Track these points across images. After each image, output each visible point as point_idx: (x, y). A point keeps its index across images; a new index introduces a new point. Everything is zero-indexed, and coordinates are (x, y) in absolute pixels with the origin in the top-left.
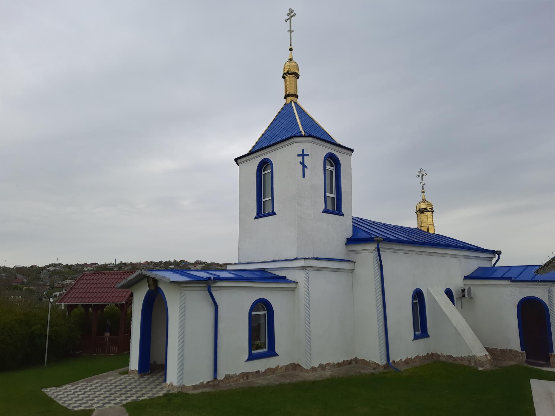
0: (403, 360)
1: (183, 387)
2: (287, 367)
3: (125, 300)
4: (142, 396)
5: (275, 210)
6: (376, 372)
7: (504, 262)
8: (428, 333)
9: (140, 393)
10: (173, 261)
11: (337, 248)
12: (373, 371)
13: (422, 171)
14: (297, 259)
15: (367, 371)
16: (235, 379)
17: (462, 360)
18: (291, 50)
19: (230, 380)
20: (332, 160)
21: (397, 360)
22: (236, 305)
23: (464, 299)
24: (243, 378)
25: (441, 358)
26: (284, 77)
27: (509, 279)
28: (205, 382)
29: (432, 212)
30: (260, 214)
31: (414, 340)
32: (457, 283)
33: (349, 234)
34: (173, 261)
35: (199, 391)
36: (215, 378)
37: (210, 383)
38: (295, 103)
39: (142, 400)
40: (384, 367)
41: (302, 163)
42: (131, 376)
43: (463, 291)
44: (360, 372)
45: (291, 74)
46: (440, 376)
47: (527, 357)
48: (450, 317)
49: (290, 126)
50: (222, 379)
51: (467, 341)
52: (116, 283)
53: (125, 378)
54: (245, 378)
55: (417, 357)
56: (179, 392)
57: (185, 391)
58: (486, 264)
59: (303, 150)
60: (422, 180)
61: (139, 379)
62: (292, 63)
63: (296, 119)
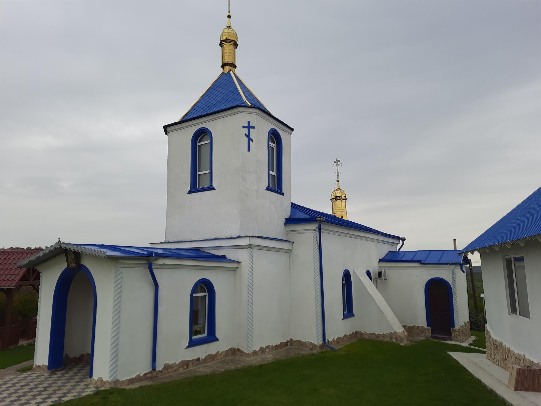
0: (335, 339)
1: (117, 381)
2: (227, 353)
3: (14, 283)
4: (65, 396)
5: (214, 185)
6: (315, 351)
7: (408, 247)
8: (354, 312)
9: (60, 393)
10: (44, 248)
11: (276, 227)
12: (310, 352)
13: (337, 161)
14: (239, 237)
15: (306, 352)
16: (175, 368)
17: (383, 337)
18: (229, 17)
19: (169, 370)
20: (275, 137)
21: (331, 340)
22: (178, 285)
23: (379, 281)
24: (183, 367)
25: (364, 336)
26: (221, 45)
27: (419, 262)
28: (142, 375)
29: (346, 200)
30: (194, 189)
31: (343, 319)
32: (374, 266)
33: (287, 213)
34: (44, 248)
35: (136, 386)
36: (154, 369)
37: (147, 376)
38: (234, 73)
39: (68, 401)
40: (321, 347)
41: (248, 136)
42: (38, 374)
43: (380, 273)
44: (299, 353)
45: (229, 42)
46: (366, 352)
47: (432, 332)
48: (373, 297)
49: (225, 97)
50: (160, 369)
51: (388, 319)
52: (19, 259)
53: (30, 376)
54: (185, 367)
55: (345, 336)
56: (112, 388)
57: (119, 386)
58: (394, 250)
59: (249, 122)
60: (338, 169)
61: (50, 376)
62: (230, 30)
63: (237, 89)
